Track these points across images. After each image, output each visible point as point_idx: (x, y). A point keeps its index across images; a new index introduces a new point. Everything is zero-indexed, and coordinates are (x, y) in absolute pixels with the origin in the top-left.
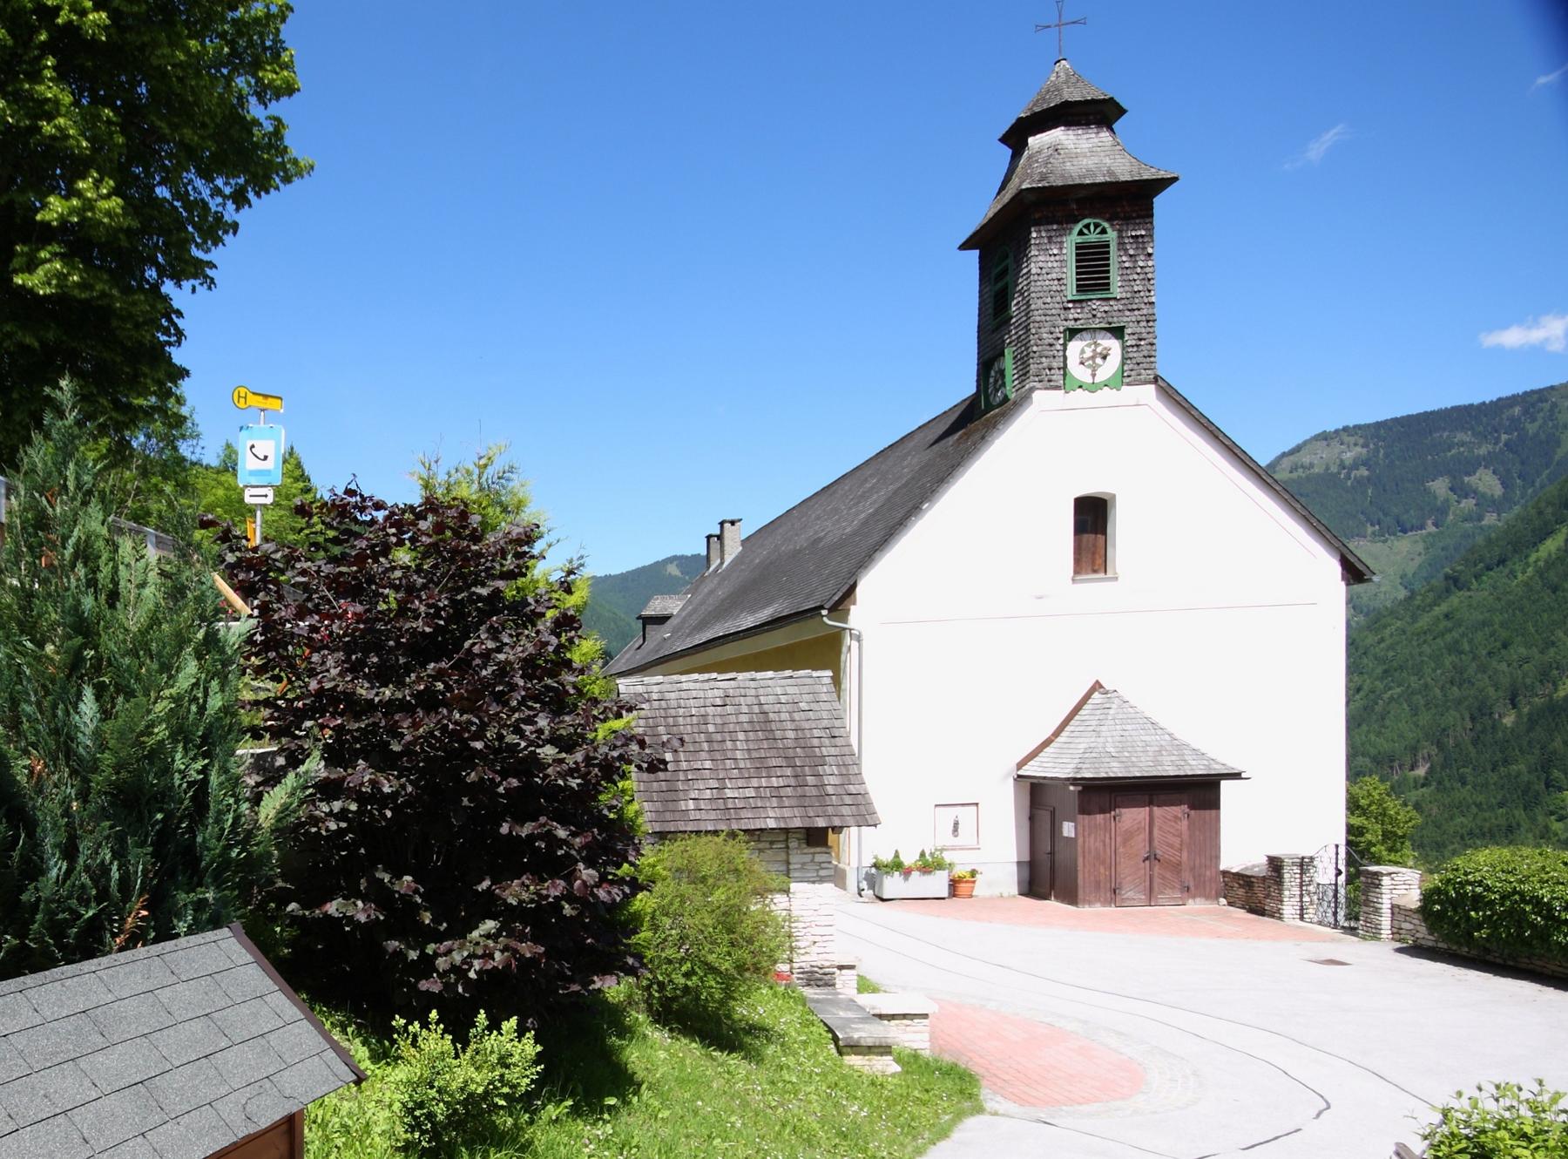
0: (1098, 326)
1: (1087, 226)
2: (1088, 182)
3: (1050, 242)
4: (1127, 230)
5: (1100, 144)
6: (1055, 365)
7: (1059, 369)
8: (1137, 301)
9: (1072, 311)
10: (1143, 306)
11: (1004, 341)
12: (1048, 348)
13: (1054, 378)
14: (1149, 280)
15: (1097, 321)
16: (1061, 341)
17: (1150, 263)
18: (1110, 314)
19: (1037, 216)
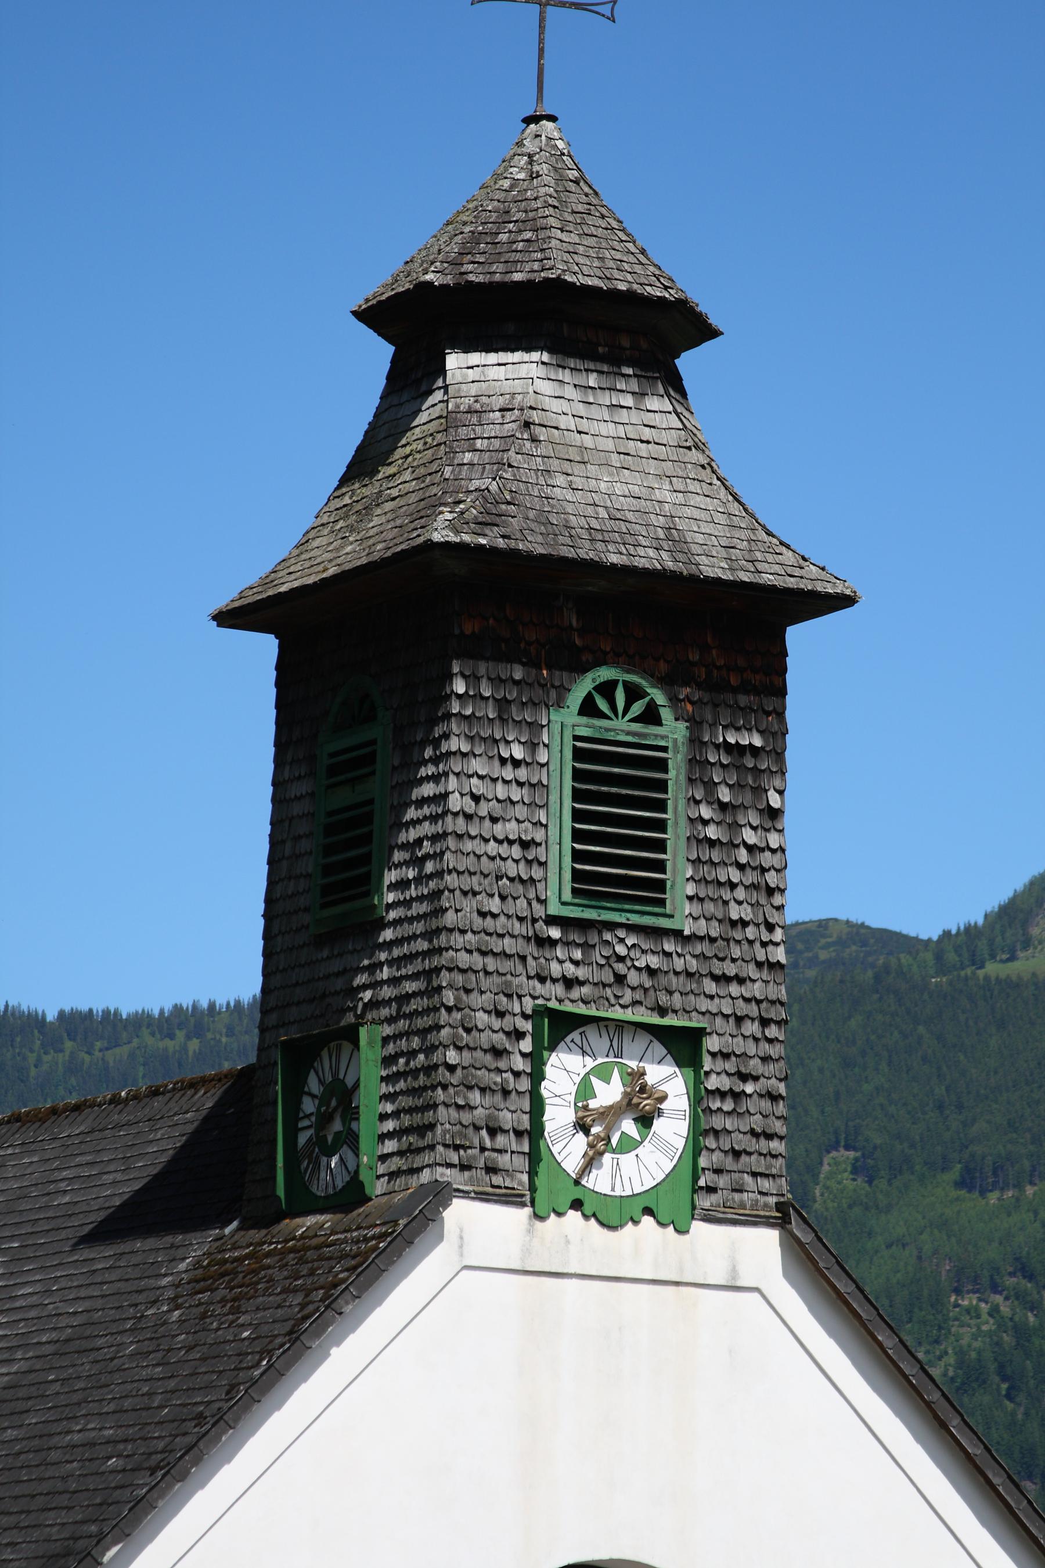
0: (628, 1015)
1: (607, 689)
2: (614, 559)
3: (503, 720)
4: (713, 725)
5: (647, 433)
6: (507, 1119)
7: (519, 1134)
8: (736, 952)
9: (560, 952)
10: (752, 971)
11: (354, 992)
12: (488, 1059)
13: (504, 1160)
14: (770, 891)
15: (628, 996)
16: (526, 1045)
17: (774, 841)
18: (663, 980)
19: (469, 628)
